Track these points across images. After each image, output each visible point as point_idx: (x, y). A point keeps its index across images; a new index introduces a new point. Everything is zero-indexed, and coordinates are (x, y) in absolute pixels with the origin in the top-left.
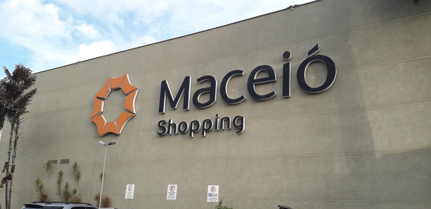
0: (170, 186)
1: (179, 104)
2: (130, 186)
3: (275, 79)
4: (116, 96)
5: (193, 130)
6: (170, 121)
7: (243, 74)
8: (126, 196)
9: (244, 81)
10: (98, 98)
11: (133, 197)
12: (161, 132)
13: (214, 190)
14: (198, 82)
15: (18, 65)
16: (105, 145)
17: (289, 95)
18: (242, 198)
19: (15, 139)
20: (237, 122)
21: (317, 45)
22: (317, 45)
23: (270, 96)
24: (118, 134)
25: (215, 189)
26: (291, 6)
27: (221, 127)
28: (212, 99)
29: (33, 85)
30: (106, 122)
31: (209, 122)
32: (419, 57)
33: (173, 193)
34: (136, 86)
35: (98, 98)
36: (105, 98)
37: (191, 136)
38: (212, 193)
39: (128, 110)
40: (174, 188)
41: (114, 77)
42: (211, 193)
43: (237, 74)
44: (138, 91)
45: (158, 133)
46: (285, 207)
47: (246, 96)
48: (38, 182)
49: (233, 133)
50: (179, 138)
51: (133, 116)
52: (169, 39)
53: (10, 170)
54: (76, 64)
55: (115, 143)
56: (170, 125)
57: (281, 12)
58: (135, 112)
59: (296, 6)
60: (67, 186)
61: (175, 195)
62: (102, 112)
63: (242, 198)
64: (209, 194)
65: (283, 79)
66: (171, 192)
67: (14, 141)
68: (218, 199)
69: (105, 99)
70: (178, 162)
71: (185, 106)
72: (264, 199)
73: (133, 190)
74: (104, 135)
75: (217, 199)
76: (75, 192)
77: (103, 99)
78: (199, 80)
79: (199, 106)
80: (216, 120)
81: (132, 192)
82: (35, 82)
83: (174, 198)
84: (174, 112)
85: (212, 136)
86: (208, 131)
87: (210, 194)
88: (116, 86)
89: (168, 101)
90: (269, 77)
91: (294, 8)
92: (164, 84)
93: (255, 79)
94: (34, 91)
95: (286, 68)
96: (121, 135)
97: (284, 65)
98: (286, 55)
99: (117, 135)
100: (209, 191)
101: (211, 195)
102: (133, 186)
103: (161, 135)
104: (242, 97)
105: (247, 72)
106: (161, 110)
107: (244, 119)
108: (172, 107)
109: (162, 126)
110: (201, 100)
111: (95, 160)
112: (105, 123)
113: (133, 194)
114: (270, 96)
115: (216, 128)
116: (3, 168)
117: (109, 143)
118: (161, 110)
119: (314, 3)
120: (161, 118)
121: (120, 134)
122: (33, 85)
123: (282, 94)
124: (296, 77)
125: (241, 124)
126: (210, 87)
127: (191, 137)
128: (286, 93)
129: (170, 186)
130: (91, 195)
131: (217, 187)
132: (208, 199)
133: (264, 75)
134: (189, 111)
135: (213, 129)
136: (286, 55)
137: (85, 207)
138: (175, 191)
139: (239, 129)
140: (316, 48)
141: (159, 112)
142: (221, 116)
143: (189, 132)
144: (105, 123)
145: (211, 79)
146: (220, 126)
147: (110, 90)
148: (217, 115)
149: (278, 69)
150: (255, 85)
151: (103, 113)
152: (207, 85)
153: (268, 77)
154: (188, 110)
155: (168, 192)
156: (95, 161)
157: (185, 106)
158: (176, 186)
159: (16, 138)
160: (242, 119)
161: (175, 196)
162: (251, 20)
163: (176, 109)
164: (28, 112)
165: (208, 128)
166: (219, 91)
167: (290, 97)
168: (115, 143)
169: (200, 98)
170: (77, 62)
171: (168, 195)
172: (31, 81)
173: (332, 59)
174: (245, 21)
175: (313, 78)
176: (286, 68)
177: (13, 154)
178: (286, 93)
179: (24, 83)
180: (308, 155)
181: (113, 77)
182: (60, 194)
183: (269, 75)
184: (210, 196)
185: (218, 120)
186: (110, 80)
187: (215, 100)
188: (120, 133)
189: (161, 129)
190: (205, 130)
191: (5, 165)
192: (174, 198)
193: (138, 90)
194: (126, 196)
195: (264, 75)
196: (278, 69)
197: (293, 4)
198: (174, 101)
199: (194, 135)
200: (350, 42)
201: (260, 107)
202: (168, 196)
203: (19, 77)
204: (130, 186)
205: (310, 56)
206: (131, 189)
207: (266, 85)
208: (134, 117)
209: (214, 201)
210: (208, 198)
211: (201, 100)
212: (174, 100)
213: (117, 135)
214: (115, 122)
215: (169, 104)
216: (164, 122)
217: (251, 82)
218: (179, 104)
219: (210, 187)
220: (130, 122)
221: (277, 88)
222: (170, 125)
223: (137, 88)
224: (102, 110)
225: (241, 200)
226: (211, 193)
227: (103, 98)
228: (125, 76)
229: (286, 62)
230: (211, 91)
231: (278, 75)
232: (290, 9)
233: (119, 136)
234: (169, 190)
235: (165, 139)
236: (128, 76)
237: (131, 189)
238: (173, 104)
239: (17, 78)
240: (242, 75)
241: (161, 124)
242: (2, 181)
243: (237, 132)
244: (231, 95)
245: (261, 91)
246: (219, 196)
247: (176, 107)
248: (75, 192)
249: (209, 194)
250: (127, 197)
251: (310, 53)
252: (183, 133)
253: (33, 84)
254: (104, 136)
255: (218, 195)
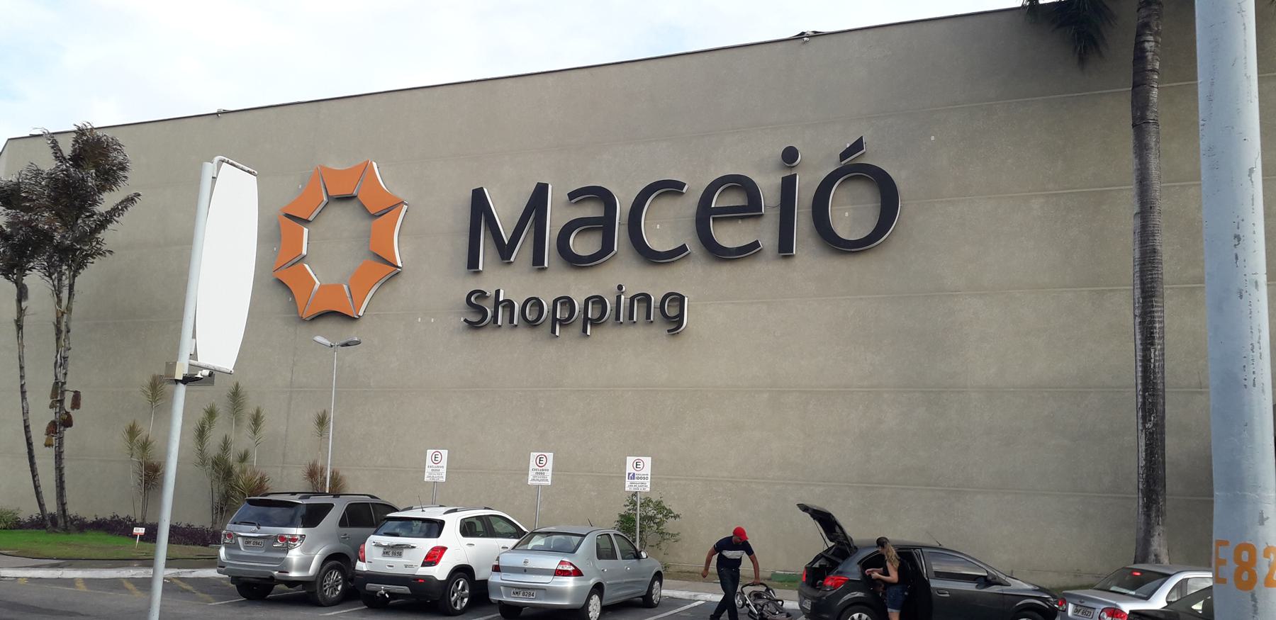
0: (534, 455)
1: (523, 249)
2: (437, 453)
3: (761, 211)
4: (342, 217)
5: (558, 320)
6: (498, 292)
7: (684, 191)
8: (426, 476)
9: (687, 206)
10: (288, 216)
11: (445, 477)
12: (474, 318)
13: (641, 466)
14: (570, 200)
15: (80, 125)
16: (332, 346)
17: (792, 252)
18: (677, 479)
19: (57, 318)
20: (668, 305)
21: (862, 138)
22: (862, 138)
23: (750, 250)
24: (356, 317)
25: (641, 463)
26: (803, 33)
27: (631, 317)
28: (607, 247)
29: (124, 181)
30: (318, 283)
31: (599, 301)
32: (1073, 189)
33: (543, 470)
34: (400, 194)
35: (288, 216)
36: (310, 219)
37: (555, 333)
38: (636, 472)
39: (378, 255)
40: (544, 459)
41: (335, 164)
42: (634, 474)
43: (672, 188)
44: (405, 207)
45: (465, 320)
46: (815, 508)
47: (693, 245)
48: (132, 432)
49: (660, 331)
50: (522, 337)
51: (395, 273)
52: (489, 77)
53: (68, 404)
54: (216, 116)
55: (358, 343)
56: (497, 303)
57: (779, 44)
58: (400, 265)
59: (817, 34)
60: (226, 446)
61: (549, 475)
62: (305, 256)
63: (677, 479)
64: (629, 474)
65: (779, 212)
66: (538, 467)
67: (54, 323)
68: (649, 486)
69: (309, 221)
70: (520, 393)
71: (538, 260)
72: (728, 481)
73: (444, 463)
74: (313, 317)
75: (648, 484)
76: (244, 458)
77: (306, 222)
78: (572, 195)
79: (574, 262)
80: (619, 298)
81: (443, 467)
82: (126, 174)
83: (547, 480)
84: (507, 271)
85: (606, 336)
86: (596, 323)
87: (631, 475)
88: (346, 192)
89: (491, 242)
90: (749, 203)
91: (813, 39)
92: (478, 196)
93: (713, 206)
94: (130, 200)
95: (788, 186)
96: (361, 320)
97: (783, 178)
98: (790, 155)
99: (351, 319)
100: (630, 469)
101: (633, 477)
102: (445, 453)
103: (473, 326)
104: (683, 249)
105: (696, 186)
106: (473, 263)
107: (686, 299)
108: (503, 258)
109: (475, 302)
110: (583, 245)
111: (292, 379)
112: (316, 287)
113: (444, 471)
114: (750, 250)
115: (618, 318)
116: (49, 397)
117: (344, 341)
118: (473, 263)
119: (859, 32)
120: (473, 284)
121: (359, 316)
122: (124, 181)
123: (777, 248)
124: (811, 210)
125: (600, 249)
126: (602, 215)
127: (553, 335)
128: (785, 247)
129: (534, 455)
130: (285, 465)
131: (647, 461)
132: (627, 486)
133: (736, 199)
134: (547, 272)
135: (610, 318)
136: (790, 155)
137: (368, 503)
138: (549, 466)
139: (675, 323)
140: (858, 146)
141: (468, 268)
142: (631, 290)
143: (549, 321)
144: (316, 287)
145: (603, 196)
146: (627, 314)
147: (325, 199)
148: (620, 287)
149: (768, 186)
150: (714, 219)
151: (306, 259)
152: (592, 210)
153: (747, 204)
154: (544, 269)
155: (531, 469)
156: (291, 382)
157: (538, 260)
158: (550, 456)
159: (60, 314)
160: (681, 299)
161: (549, 478)
162: (706, 56)
163: (512, 262)
164: (111, 252)
165: (597, 316)
166: (625, 228)
167: (793, 256)
168: (358, 343)
169: (576, 239)
170: (216, 111)
171: (531, 474)
172: (114, 171)
173: (892, 173)
174: (689, 56)
175: (847, 214)
176: (788, 186)
177: (56, 357)
178: (785, 247)
179: (95, 173)
180: (829, 389)
181: (330, 165)
182: (203, 463)
183: (747, 201)
184: (631, 479)
185: (623, 297)
186: (323, 174)
187: (615, 249)
188: (361, 314)
189: (474, 310)
190: (589, 321)
191: (52, 390)
192: (547, 480)
193: (406, 204)
194: (426, 474)
195: (736, 199)
196: (768, 186)
197: (809, 29)
198: (506, 242)
199: (562, 330)
200: (933, 138)
201: (725, 273)
202: (530, 477)
203: (87, 160)
204: (437, 453)
205: (843, 163)
206: (439, 459)
207: (740, 222)
208: (398, 276)
209: (641, 489)
210: (628, 482)
211: (583, 245)
212: (506, 242)
213: (351, 319)
214: (345, 286)
215: (493, 249)
216: (482, 295)
217: (705, 215)
218: (523, 249)
219: (630, 460)
220: (387, 289)
221: (765, 232)
222: (497, 303)
223: (403, 202)
224: (304, 252)
225: (676, 482)
226: (634, 474)
227: (306, 218)
228: (366, 168)
229: (788, 174)
230: (604, 226)
231: (765, 195)
232: (801, 41)
233: (358, 322)
234: (533, 465)
235: (484, 336)
236: (375, 165)
237: (439, 459)
238: (505, 251)
239: (81, 164)
240: (683, 193)
241: (473, 299)
242: (48, 433)
243: (669, 331)
244: (657, 240)
245: (728, 235)
246: (651, 478)
247: (512, 260)
248: (244, 458)
249: (629, 474)
250: (428, 477)
251: (844, 156)
252: (533, 324)
253: (124, 179)
254: (313, 319)
255: (649, 477)
